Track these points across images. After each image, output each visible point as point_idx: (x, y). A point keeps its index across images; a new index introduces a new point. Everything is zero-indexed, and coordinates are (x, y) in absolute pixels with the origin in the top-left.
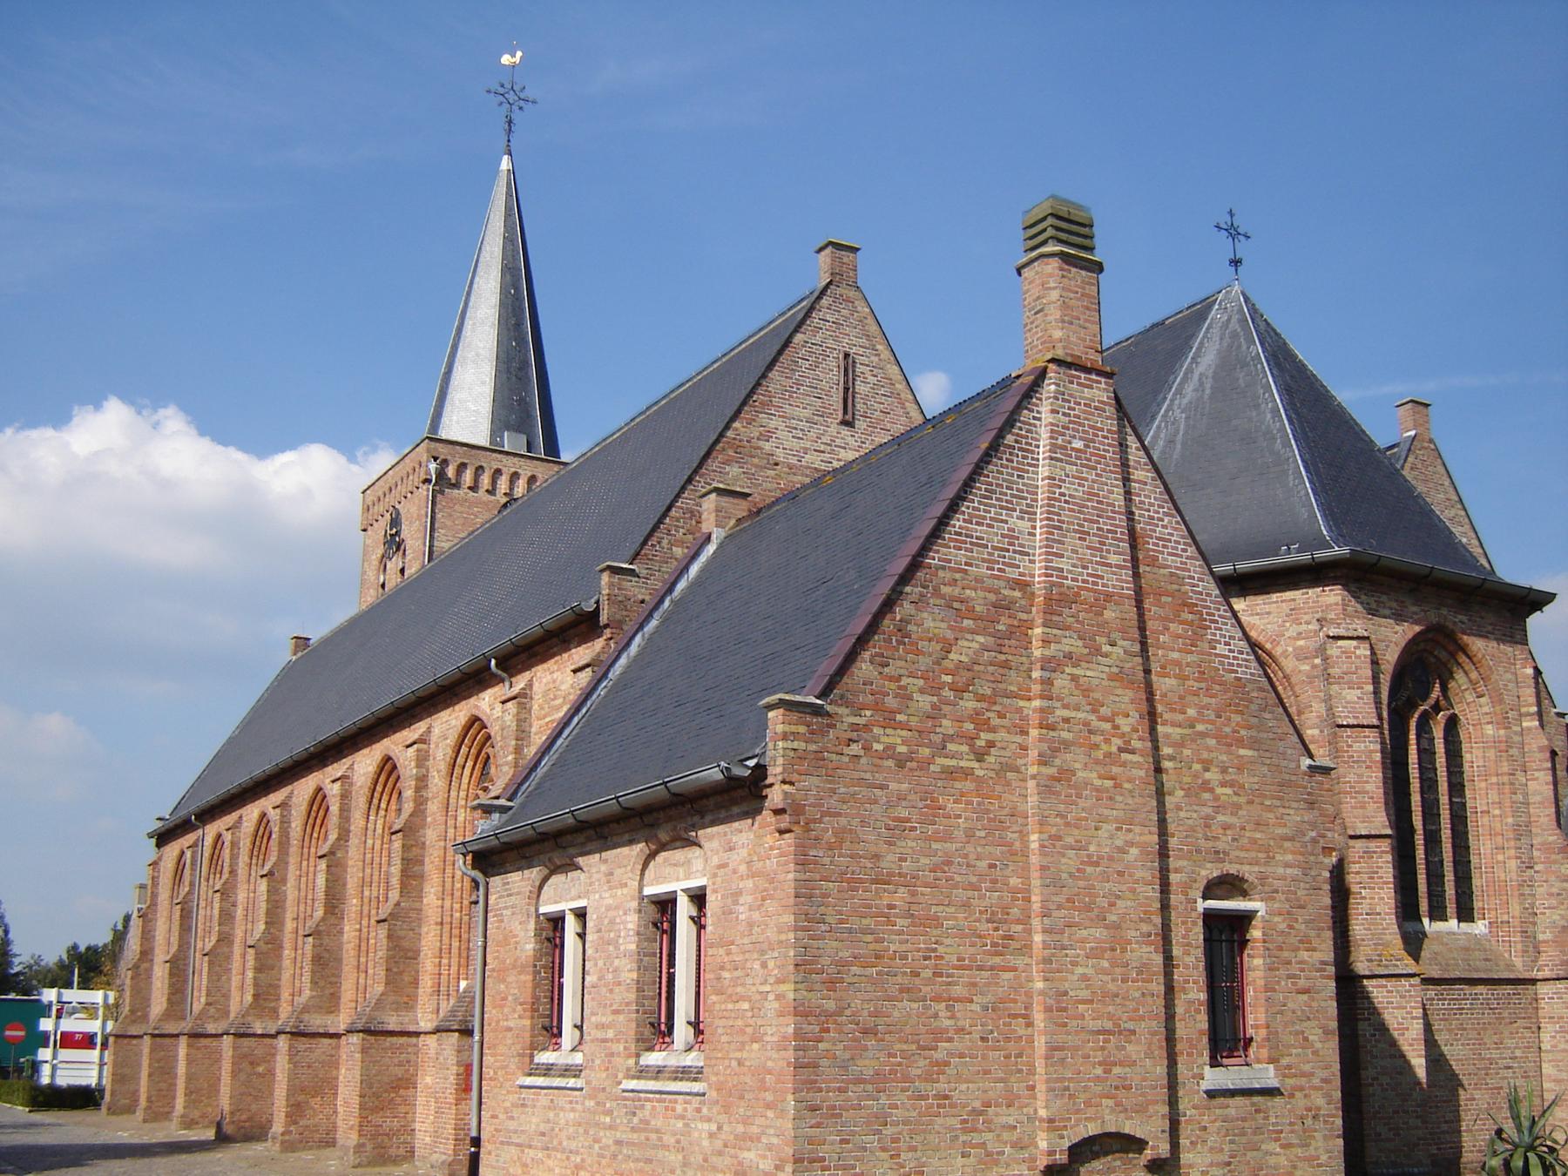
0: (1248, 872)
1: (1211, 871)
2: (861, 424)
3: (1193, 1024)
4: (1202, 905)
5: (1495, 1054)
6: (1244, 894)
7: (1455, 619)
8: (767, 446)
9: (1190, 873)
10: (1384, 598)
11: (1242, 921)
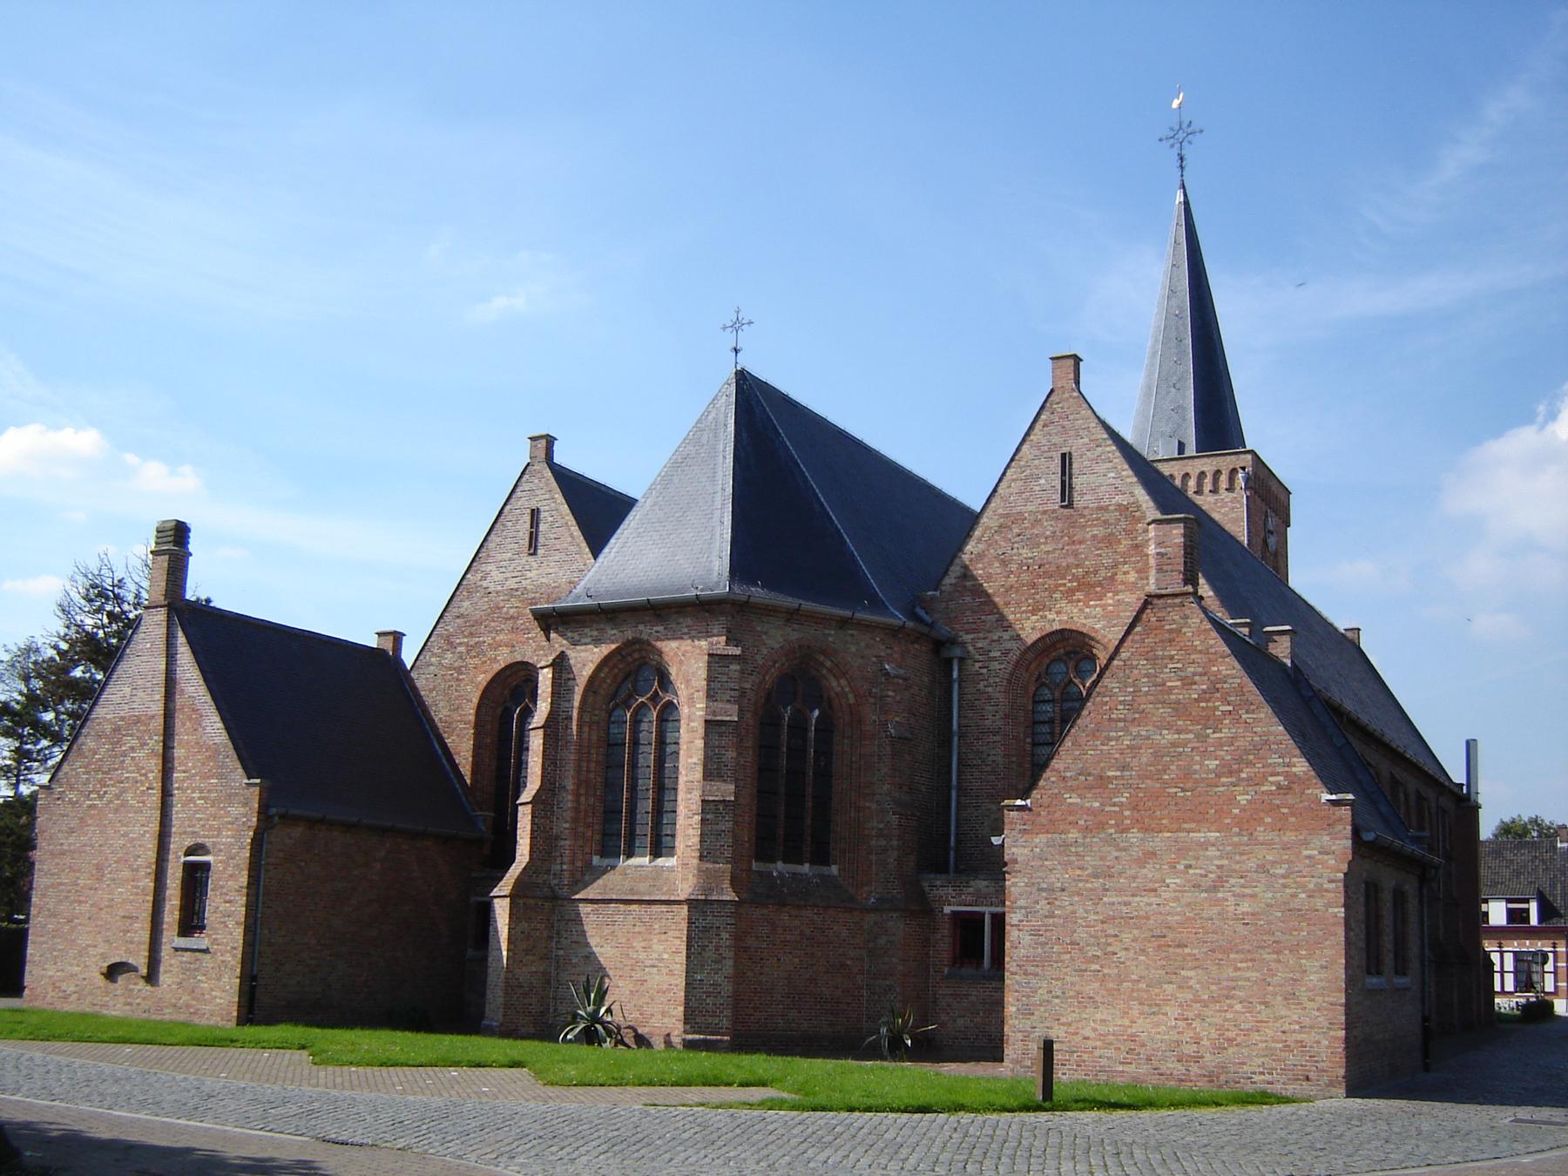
0: (208, 842)
1: (189, 842)
2: (540, 552)
3: (171, 915)
4: (183, 859)
5: (642, 956)
6: (207, 853)
7: (645, 631)
8: (485, 584)
9: (178, 845)
10: (587, 630)
11: (206, 867)
